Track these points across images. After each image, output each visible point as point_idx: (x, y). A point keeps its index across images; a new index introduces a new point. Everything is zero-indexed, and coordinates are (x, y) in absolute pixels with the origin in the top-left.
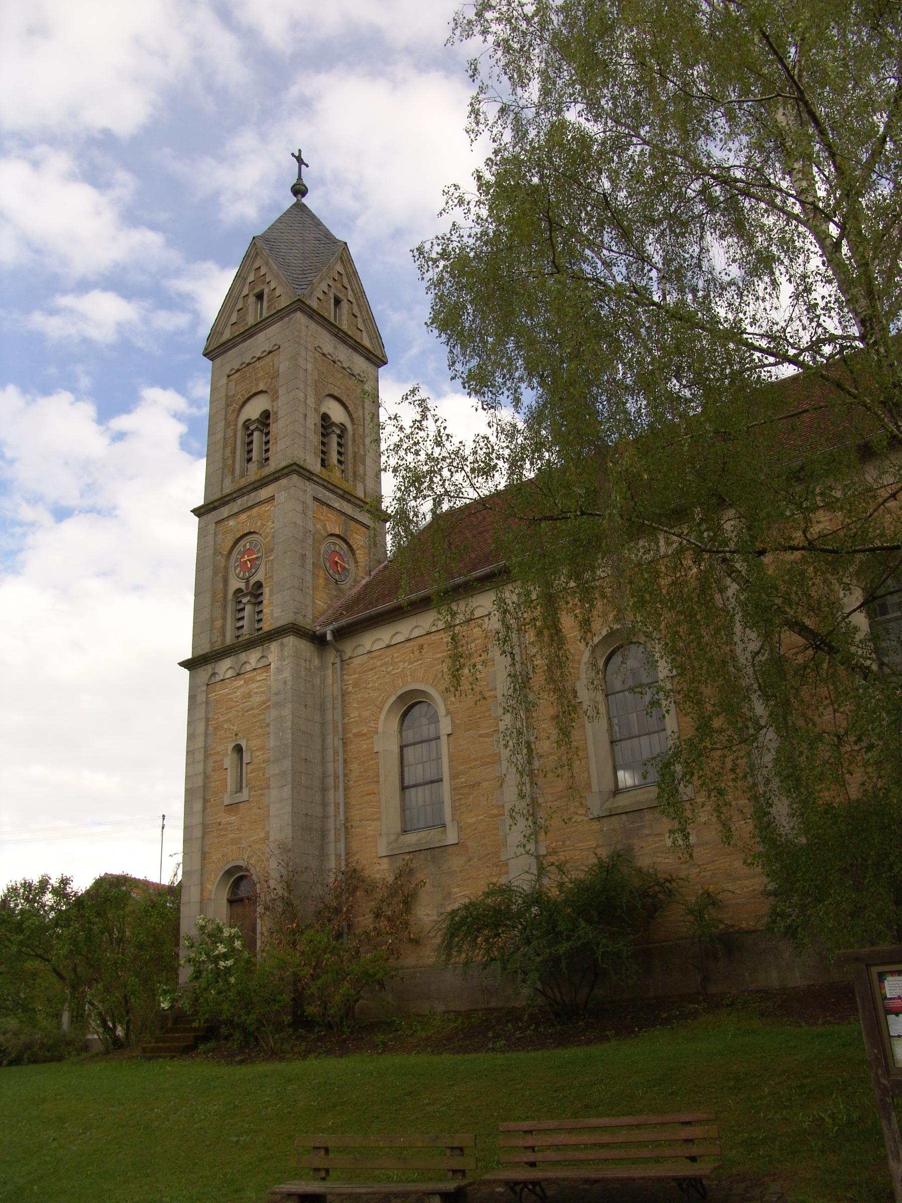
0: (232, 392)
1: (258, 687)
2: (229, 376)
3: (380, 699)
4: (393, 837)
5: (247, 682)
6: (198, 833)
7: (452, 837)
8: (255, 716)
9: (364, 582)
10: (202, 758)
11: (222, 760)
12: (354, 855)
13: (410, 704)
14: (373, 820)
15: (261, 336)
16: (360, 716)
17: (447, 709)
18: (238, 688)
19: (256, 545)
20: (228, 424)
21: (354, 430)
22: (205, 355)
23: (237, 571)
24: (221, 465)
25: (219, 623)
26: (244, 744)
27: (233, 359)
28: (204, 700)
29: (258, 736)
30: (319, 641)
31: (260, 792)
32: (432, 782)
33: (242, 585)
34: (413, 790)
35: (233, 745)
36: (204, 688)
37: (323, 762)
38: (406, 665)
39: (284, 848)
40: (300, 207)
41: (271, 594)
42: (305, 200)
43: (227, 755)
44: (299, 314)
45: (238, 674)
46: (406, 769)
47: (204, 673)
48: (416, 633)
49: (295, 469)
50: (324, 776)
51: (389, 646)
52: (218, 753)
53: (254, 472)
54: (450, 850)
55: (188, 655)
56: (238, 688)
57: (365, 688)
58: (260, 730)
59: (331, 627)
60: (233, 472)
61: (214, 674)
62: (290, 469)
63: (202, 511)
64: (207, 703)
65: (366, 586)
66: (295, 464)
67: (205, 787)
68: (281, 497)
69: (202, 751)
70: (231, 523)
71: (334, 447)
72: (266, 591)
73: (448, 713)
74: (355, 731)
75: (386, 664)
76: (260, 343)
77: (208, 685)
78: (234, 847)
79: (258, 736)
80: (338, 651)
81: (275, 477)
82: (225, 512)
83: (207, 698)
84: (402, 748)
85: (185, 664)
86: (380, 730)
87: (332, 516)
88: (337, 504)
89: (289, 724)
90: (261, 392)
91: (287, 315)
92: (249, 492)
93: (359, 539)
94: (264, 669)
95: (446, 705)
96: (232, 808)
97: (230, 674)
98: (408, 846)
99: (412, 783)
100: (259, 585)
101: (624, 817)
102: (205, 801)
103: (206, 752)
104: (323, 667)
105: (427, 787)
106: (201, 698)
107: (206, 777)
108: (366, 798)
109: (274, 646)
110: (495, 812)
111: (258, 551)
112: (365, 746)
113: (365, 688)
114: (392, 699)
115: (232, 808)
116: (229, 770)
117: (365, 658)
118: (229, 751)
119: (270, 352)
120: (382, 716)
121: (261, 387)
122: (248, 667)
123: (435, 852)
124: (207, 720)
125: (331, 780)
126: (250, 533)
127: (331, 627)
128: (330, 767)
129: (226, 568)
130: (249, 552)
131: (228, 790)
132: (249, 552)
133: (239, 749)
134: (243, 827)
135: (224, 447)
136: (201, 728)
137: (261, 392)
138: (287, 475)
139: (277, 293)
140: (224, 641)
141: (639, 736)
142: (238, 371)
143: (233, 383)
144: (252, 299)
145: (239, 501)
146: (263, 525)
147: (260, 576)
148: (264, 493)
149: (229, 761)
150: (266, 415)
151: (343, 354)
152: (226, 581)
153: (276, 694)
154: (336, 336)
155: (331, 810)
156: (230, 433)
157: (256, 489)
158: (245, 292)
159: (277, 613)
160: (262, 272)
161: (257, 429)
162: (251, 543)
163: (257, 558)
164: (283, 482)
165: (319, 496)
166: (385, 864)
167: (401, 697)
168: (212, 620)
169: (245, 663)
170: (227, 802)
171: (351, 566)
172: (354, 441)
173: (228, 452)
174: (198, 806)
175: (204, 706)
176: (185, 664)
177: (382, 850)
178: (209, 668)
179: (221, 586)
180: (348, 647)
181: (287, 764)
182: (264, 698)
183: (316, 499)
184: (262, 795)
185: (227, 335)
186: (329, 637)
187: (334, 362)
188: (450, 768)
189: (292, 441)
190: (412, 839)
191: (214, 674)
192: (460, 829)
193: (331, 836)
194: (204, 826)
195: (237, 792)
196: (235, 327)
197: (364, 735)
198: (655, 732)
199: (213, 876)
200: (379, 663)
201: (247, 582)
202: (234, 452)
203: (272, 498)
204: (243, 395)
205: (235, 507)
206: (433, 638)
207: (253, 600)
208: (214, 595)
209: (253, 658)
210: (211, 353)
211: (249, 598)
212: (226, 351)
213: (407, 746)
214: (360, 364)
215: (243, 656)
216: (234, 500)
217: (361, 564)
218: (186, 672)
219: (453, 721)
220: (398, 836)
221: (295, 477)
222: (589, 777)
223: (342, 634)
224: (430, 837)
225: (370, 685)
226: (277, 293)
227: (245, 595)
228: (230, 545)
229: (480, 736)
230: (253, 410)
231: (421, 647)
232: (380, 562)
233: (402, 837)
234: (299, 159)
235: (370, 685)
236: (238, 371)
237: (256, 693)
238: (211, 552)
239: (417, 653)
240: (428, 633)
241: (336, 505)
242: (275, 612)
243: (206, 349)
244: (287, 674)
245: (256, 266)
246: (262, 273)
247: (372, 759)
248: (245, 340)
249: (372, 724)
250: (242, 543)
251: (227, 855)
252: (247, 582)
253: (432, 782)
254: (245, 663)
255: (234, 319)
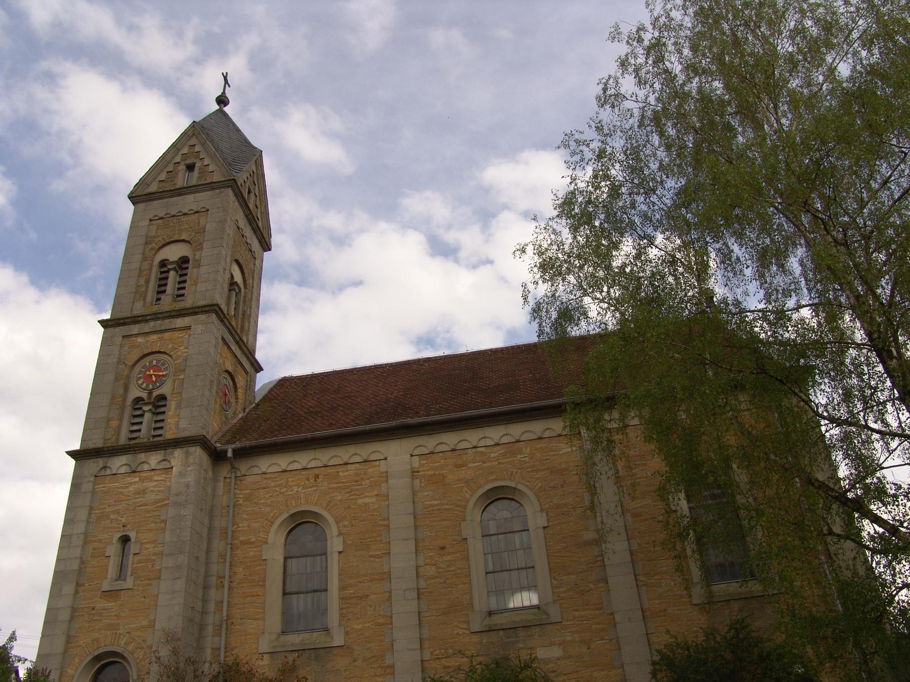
0: (153, 234)
1: (154, 487)
2: (151, 220)
3: (272, 515)
4: (274, 636)
5: (142, 480)
6: (65, 615)
7: (338, 639)
8: (148, 512)
9: (240, 416)
10: (80, 542)
11: (105, 548)
12: (232, 650)
13: (301, 522)
14: (255, 619)
15: (190, 198)
16: (249, 526)
17: (339, 531)
18: (131, 484)
19: (163, 364)
20: (145, 259)
21: (245, 293)
22: (131, 197)
23: (140, 382)
24: (134, 290)
25: (115, 423)
26: (133, 535)
27: (158, 208)
28: (91, 489)
29: (150, 530)
30: (217, 457)
31: (147, 582)
32: (315, 591)
33: (144, 395)
34: (294, 597)
35: (120, 535)
36: (92, 479)
37: (207, 563)
38: (300, 489)
39: (170, 637)
40: (221, 112)
41: (179, 407)
42: (226, 109)
43: (111, 543)
44: (230, 190)
45: (134, 472)
46: (288, 578)
47: (93, 466)
48: (313, 464)
49: (212, 309)
50: (207, 575)
51: (284, 471)
52: (100, 541)
53: (167, 302)
54: (335, 651)
55: (76, 446)
56: (131, 484)
57: (257, 503)
58: (153, 525)
59: (233, 446)
60: (145, 299)
61: (105, 467)
62: (212, 308)
63: (110, 323)
64: (93, 492)
65: (242, 419)
66: (217, 305)
67: (80, 572)
68: (198, 329)
69: (82, 537)
70: (140, 340)
71: (233, 299)
72: (172, 405)
73: (340, 534)
74: (242, 538)
75: (279, 485)
76: (189, 202)
77: (96, 476)
78: (109, 633)
79: (150, 530)
80: (233, 467)
81: (194, 311)
82: (135, 329)
83: (94, 489)
84: (286, 559)
85: (72, 454)
86: (270, 540)
87: (229, 356)
88: (234, 347)
89: (189, 523)
90: (183, 241)
91: (219, 188)
92: (164, 318)
93: (241, 381)
94: (164, 471)
95: (338, 527)
96: (111, 594)
97: (123, 470)
98: (292, 644)
99: (294, 590)
100: (163, 398)
101: (501, 633)
102: (78, 585)
103: (86, 537)
104: (215, 480)
105: (309, 595)
106: (87, 487)
107: (82, 562)
108: (249, 599)
109: (178, 453)
110: (382, 621)
111: (166, 369)
112: (252, 553)
113: (257, 503)
114: (286, 515)
115: (111, 594)
116: (112, 558)
117: (259, 478)
118: (115, 541)
119: (198, 212)
120: (273, 529)
121: (184, 236)
122: (146, 467)
123: (320, 653)
124: (91, 509)
125: (213, 580)
126: (164, 353)
127: (233, 446)
128: (214, 568)
129: (128, 377)
130: (157, 368)
131: (109, 576)
132: (157, 368)
133: (125, 540)
134: (122, 614)
135: (139, 276)
136: (83, 515)
137: (183, 241)
138: (206, 312)
139: (211, 168)
140: (117, 439)
141: (510, 570)
142: (162, 218)
143: (155, 227)
144: (182, 167)
145: (152, 323)
146: (174, 349)
147: (165, 390)
148: (180, 322)
149: (113, 550)
150: (185, 260)
151: (248, 232)
152: (126, 388)
153: (177, 495)
154: (247, 217)
155: (211, 607)
156: (146, 265)
157: (172, 317)
158: (178, 159)
159: (183, 424)
160: (197, 149)
161: (174, 269)
162: (158, 361)
163: (163, 376)
164: (202, 317)
165: (225, 337)
166: (266, 660)
167: (293, 516)
168: (109, 420)
169: (143, 463)
170: (106, 587)
171: (233, 400)
172: (245, 301)
173: (142, 281)
174: (69, 589)
175: (90, 495)
176: (72, 454)
177: (264, 646)
178: (101, 462)
179: (121, 391)
180: (243, 466)
181: (183, 559)
182: (161, 497)
183: (223, 339)
184: (150, 585)
185: (154, 188)
186: (230, 454)
187: (243, 236)
188: (340, 580)
189: (206, 286)
190: (294, 639)
191: (105, 467)
192: (347, 633)
193: (210, 630)
194: (74, 610)
195: (116, 580)
196: (162, 184)
197: (253, 543)
198: (523, 568)
199: (77, 660)
200: (273, 484)
201: (150, 393)
202: (147, 282)
203: (189, 328)
204: (163, 239)
205: (147, 327)
206: (329, 470)
207: (153, 410)
208: (113, 398)
209: (154, 459)
210: (134, 198)
211: (150, 407)
212: (150, 200)
213: (291, 558)
214: (256, 245)
215: (142, 457)
216: (147, 321)
217: (240, 401)
218: (72, 462)
219: (344, 541)
220: (279, 635)
221: (214, 316)
222: (471, 598)
223: (243, 453)
224: (316, 639)
225: (262, 501)
226: (211, 168)
227: (146, 404)
228: (136, 358)
229: (371, 556)
230: (173, 253)
231: (317, 476)
232: (251, 404)
233: (283, 638)
234: (225, 78)
235: (262, 501)
236: (162, 218)
237: (152, 491)
238: (115, 360)
239: (312, 481)
240: (326, 466)
241: (233, 348)
242: (177, 422)
243: (132, 193)
244: (191, 479)
245: (192, 142)
246: (196, 150)
247: (260, 565)
248: (172, 197)
249: (261, 535)
250: (148, 359)
251: (94, 640)
252: (150, 393)
253: (315, 591)
254: (143, 463)
255: (163, 177)
